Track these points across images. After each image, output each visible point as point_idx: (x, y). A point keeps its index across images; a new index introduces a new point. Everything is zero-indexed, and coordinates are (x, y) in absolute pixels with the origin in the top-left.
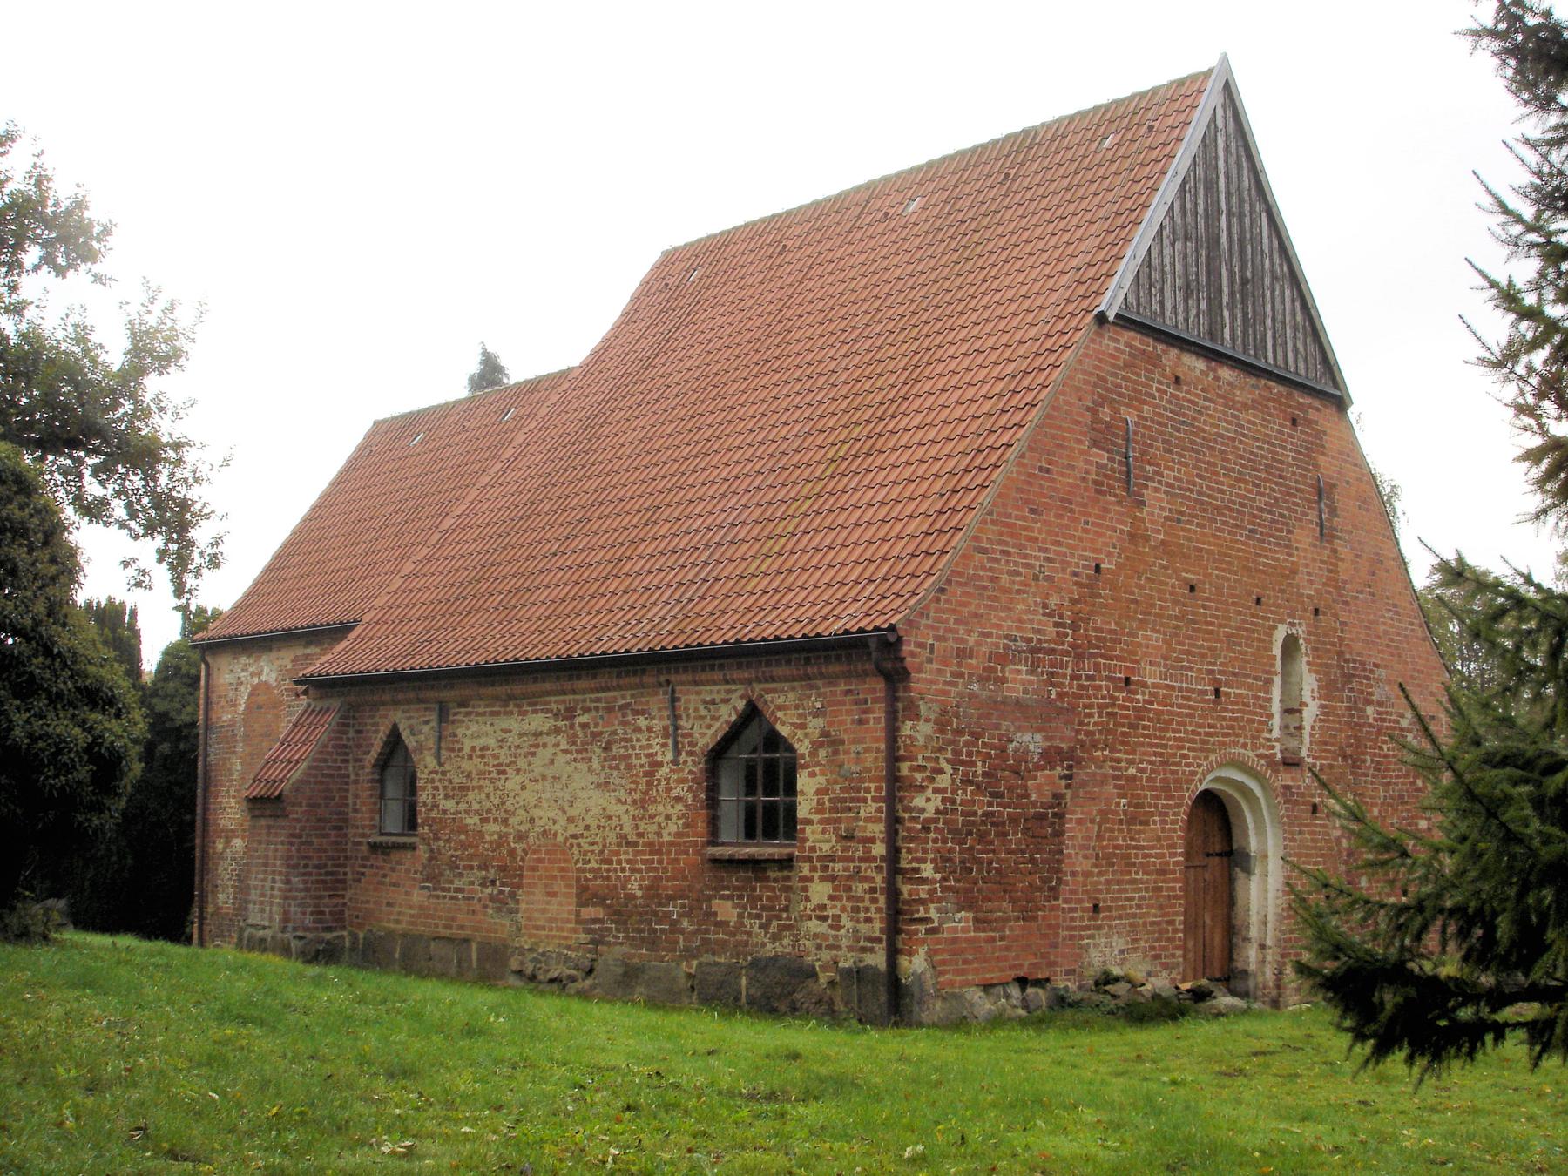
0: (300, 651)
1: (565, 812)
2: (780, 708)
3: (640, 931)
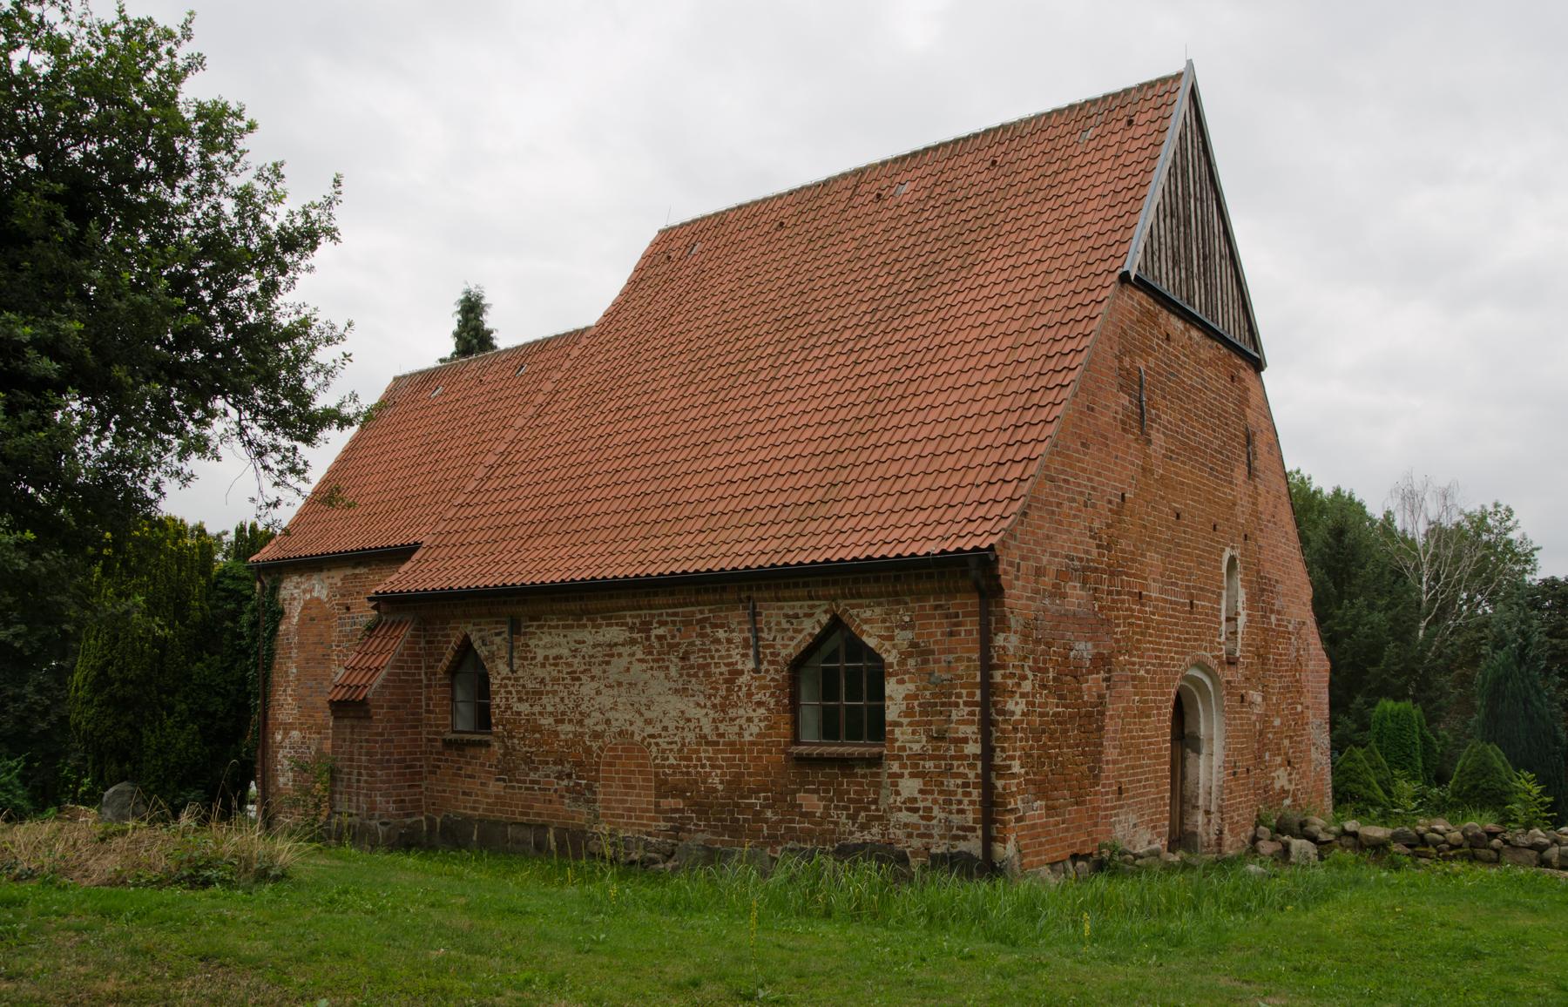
0: (349, 572)
1: (641, 715)
2: (866, 621)
3: (721, 820)
